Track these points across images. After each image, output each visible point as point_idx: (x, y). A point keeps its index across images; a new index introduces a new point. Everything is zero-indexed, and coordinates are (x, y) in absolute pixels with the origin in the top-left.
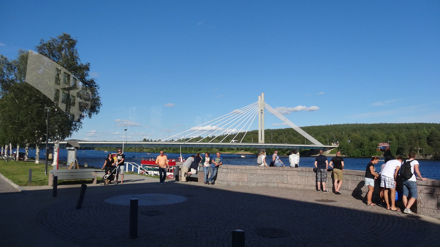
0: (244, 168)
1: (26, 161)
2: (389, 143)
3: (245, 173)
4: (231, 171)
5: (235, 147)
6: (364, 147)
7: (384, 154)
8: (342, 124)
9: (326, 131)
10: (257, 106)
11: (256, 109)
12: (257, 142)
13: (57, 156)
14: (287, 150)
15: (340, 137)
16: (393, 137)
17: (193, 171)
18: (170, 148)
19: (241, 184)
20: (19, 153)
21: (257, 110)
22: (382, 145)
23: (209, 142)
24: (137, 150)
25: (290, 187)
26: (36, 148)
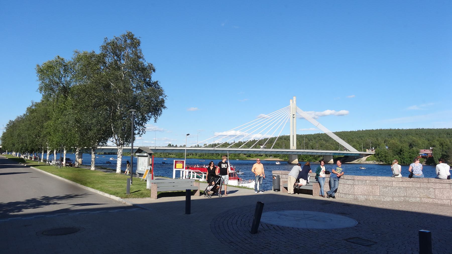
0: (375, 179)
1: (77, 167)
2: (432, 150)
3: (377, 185)
4: (359, 183)
5: (102, 151)
6: (403, 154)
7: (426, 162)
8: (375, 129)
9: (359, 137)
10: (288, 110)
11: (287, 114)
12: (289, 148)
13: (120, 163)
14: (319, 156)
15: (376, 143)
16: (437, 143)
17: (303, 182)
18: (196, 153)
19: (371, 198)
20: (66, 158)
21: (288, 114)
22: (423, 152)
24: (162, 156)
25: (439, 202)
26: (91, 153)
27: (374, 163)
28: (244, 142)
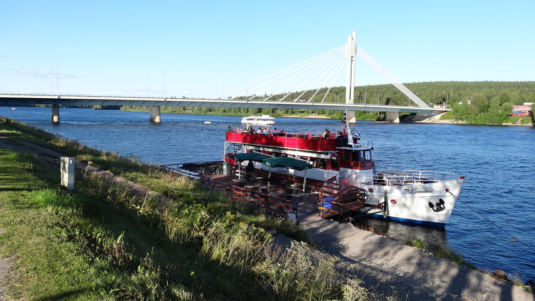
12: (344, 101)
23: (280, 101)
27: (451, 123)
28: (302, 93)
